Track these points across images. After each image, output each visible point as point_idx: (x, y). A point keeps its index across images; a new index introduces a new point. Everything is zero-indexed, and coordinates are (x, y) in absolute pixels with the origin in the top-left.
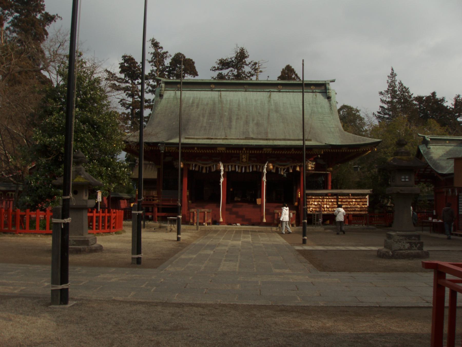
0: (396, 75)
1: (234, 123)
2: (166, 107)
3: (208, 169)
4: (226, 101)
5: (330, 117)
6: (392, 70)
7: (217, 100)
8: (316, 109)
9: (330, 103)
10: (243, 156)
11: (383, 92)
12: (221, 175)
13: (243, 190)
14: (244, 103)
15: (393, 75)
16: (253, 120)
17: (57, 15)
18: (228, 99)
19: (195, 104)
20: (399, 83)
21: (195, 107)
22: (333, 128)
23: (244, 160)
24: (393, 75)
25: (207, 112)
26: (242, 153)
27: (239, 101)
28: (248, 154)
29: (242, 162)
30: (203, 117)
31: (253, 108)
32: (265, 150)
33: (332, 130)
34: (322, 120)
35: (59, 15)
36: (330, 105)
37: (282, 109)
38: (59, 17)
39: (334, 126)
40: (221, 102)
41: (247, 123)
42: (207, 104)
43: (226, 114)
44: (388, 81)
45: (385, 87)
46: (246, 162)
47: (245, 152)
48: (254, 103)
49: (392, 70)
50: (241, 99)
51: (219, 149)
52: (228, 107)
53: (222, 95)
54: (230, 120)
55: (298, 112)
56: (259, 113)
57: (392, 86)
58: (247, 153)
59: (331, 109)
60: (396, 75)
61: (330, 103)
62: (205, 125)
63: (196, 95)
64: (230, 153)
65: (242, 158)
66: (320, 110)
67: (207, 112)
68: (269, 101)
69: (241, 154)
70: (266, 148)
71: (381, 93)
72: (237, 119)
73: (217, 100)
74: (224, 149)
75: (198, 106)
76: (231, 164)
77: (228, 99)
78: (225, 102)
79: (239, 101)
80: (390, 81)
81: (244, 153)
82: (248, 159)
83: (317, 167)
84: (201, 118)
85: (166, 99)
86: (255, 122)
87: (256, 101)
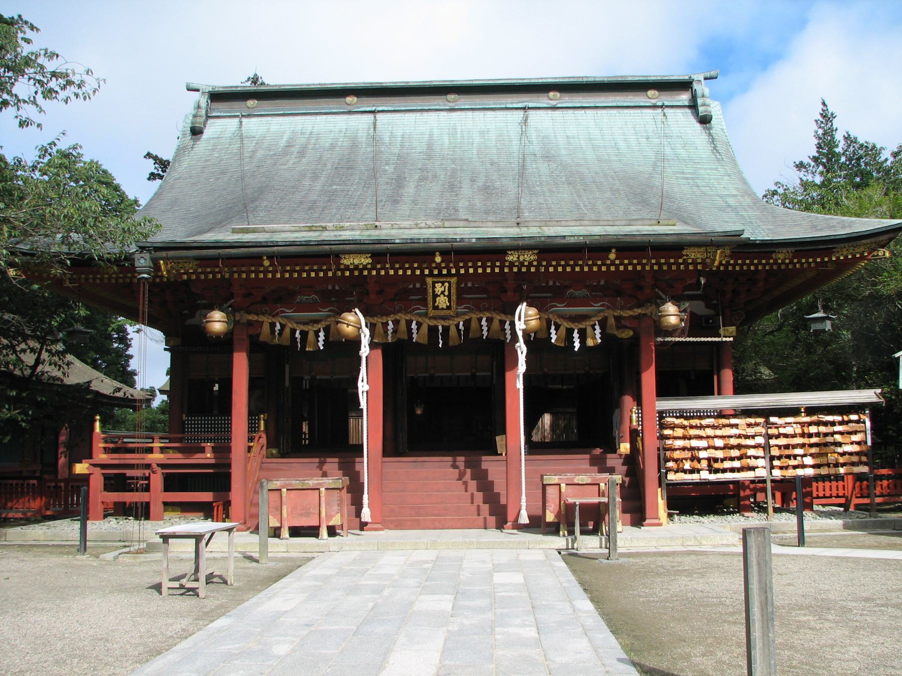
0: (833, 116)
1: (410, 189)
2: (207, 161)
3: (761, 485)
4: (392, 136)
5: (716, 169)
6: (824, 104)
7: (362, 137)
8: (668, 151)
9: (710, 135)
10: (439, 288)
11: (806, 161)
12: (360, 358)
13: (445, 414)
14: (447, 141)
15: (827, 117)
16: (473, 181)
17: (20, 16)
18: (399, 133)
19: (295, 150)
20: (846, 138)
21: (295, 154)
22: (734, 196)
23: (442, 301)
24: (827, 117)
25: (329, 166)
26: (431, 274)
27: (431, 136)
28: (454, 280)
29: (436, 308)
30: (315, 177)
31: (475, 152)
32: (512, 257)
33: (731, 201)
34: (692, 179)
35: (24, 18)
36: (713, 141)
37: (563, 152)
38: (26, 23)
39: (734, 192)
40: (375, 140)
41: (452, 187)
42: (333, 147)
43: (390, 169)
44: (816, 132)
45: (808, 149)
46: (449, 308)
47: (445, 272)
48: (477, 139)
49: (824, 104)
50: (435, 131)
51: (347, 261)
52: (396, 151)
53: (378, 123)
54: (399, 182)
55: (615, 158)
56: (492, 164)
57: (826, 142)
58: (449, 274)
59: (715, 148)
60: (833, 116)
61: (710, 135)
62: (313, 197)
63: (299, 128)
64: (392, 275)
65: (435, 296)
66: (682, 153)
67: (329, 166)
68: (523, 133)
69: (429, 281)
70: (517, 249)
71: (800, 166)
72: (423, 179)
73: (362, 137)
74: (365, 260)
75: (302, 153)
76: (393, 317)
77: (399, 133)
78: (387, 140)
79: (431, 136)
80: (820, 132)
81: (440, 274)
82: (454, 298)
83: (696, 324)
84: (307, 183)
85: (209, 139)
86: (480, 182)
87: (482, 133)
